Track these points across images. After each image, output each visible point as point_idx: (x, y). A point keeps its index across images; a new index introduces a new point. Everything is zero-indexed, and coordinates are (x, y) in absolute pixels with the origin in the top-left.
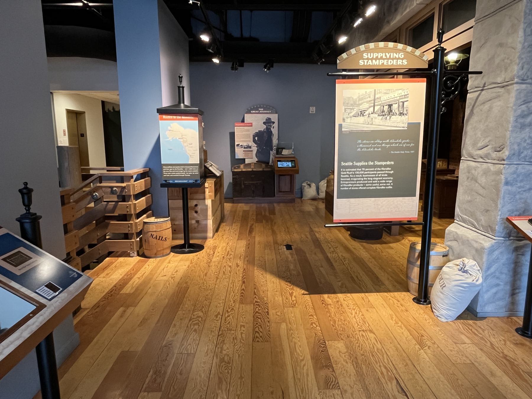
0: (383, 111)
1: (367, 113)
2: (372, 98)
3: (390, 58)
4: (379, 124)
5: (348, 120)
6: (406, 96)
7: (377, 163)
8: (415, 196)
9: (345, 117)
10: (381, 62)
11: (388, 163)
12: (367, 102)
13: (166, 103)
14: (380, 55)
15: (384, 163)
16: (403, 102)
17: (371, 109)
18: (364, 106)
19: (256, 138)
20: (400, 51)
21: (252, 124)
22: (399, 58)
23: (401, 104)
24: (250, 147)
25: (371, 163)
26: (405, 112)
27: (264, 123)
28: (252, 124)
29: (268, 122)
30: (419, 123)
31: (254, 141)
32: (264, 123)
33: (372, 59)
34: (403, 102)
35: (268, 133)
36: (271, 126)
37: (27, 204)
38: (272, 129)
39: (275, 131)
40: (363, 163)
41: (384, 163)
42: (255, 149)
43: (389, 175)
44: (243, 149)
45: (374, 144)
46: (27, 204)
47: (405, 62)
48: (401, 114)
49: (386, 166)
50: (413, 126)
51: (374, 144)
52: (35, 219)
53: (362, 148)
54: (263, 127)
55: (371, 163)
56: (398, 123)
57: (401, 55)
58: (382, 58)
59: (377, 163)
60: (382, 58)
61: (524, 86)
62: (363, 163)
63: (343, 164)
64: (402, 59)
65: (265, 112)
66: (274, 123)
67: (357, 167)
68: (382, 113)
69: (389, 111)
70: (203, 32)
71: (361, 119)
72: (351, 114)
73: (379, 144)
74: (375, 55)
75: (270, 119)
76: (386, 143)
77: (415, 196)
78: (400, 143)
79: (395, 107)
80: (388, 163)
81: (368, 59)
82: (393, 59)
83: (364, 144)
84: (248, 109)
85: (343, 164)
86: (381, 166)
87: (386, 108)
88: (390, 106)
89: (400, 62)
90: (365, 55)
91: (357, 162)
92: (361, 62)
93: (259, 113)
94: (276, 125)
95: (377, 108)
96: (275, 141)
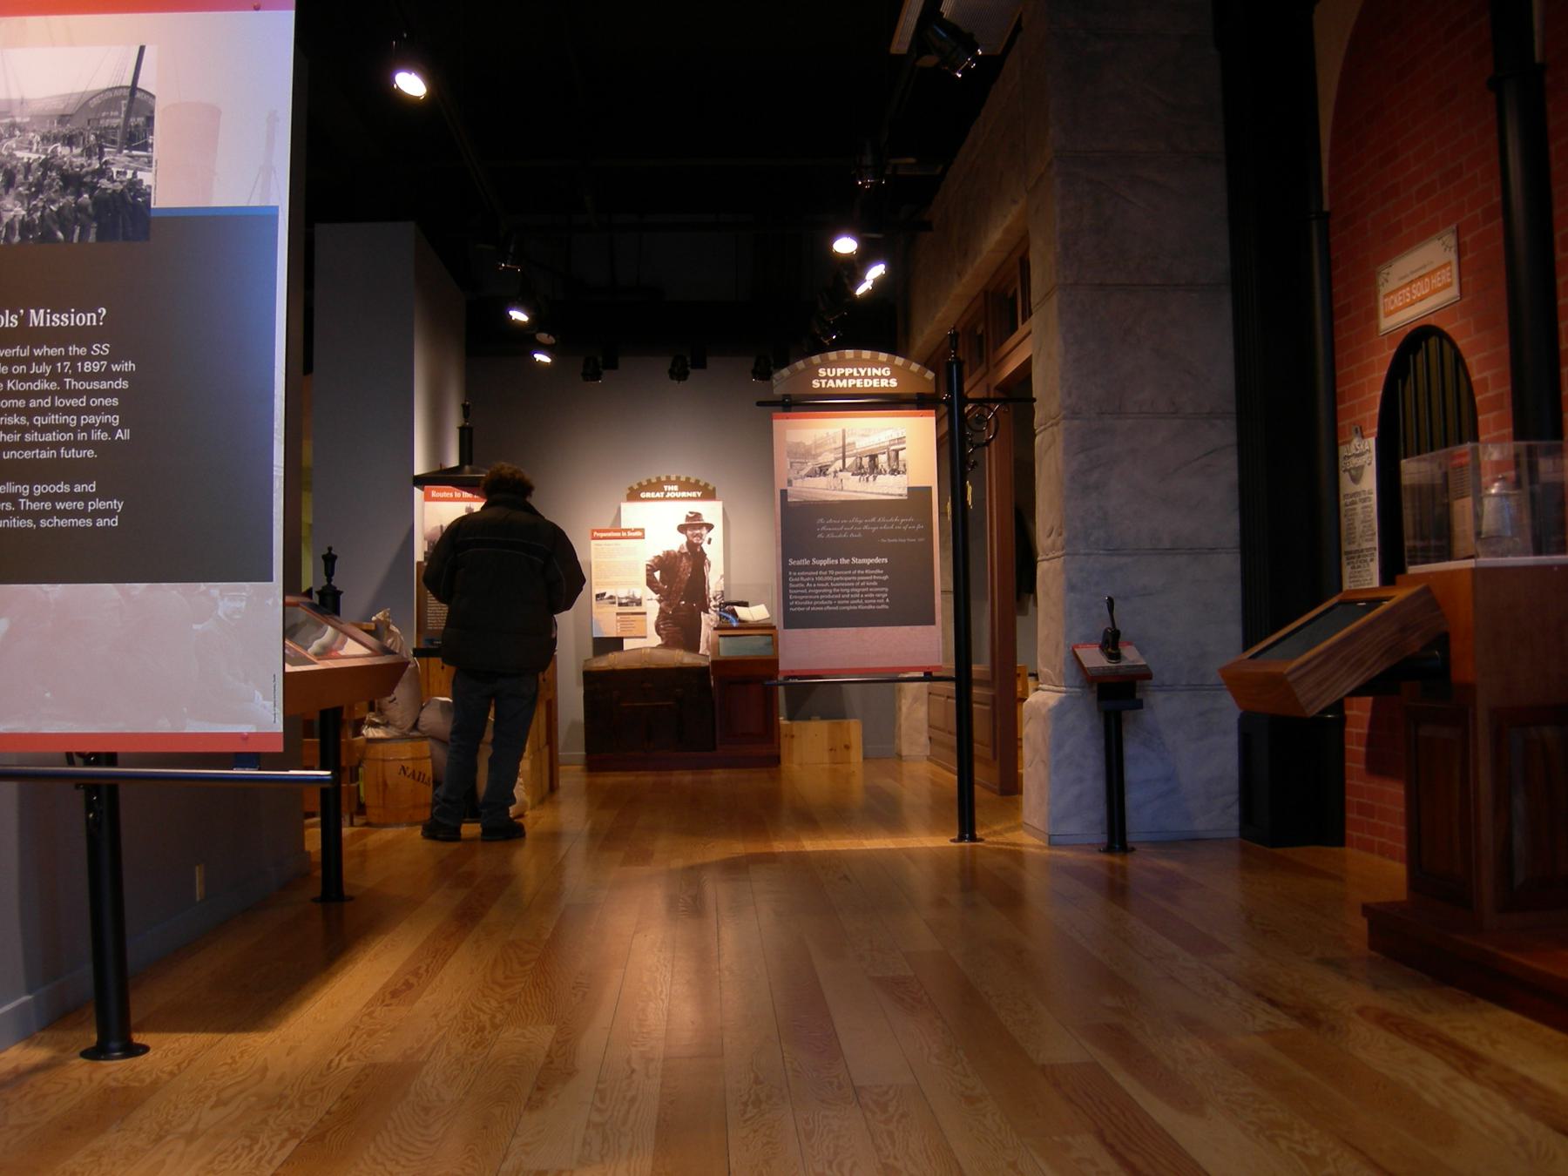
0: (861, 467)
1: (831, 470)
2: (840, 444)
3: (866, 376)
4: (855, 488)
5: (797, 484)
6: (901, 440)
7: (855, 561)
8: (933, 623)
9: (791, 476)
10: (851, 382)
11: (877, 560)
12: (831, 451)
13: (419, 469)
14: (848, 371)
15: (869, 561)
16: (897, 452)
17: (839, 464)
18: (826, 458)
19: (657, 574)
20: (882, 365)
21: (642, 530)
22: (883, 377)
23: (893, 454)
24: (639, 603)
25: (844, 561)
26: (901, 468)
27: (682, 529)
28: (642, 530)
29: (693, 524)
30: (930, 488)
31: (651, 583)
32: (682, 529)
33: (835, 378)
34: (897, 452)
35: (696, 556)
36: (701, 536)
37: (330, 573)
38: (705, 546)
39: (714, 550)
40: (828, 561)
41: (869, 561)
42: (652, 606)
43: (881, 583)
44: (616, 608)
45: (848, 525)
46: (330, 573)
47: (894, 383)
48: (894, 472)
49: (873, 566)
50: (918, 495)
51: (848, 525)
52: (336, 594)
53: (825, 533)
54: (677, 542)
55: (844, 561)
56: (888, 487)
57: (886, 371)
58: (851, 376)
59: (855, 561)
60: (851, 376)
61: (1076, 422)
62: (828, 561)
63: (792, 562)
64: (888, 378)
65: (684, 494)
66: (710, 527)
67: (817, 568)
68: (859, 471)
69: (870, 466)
70: (409, 66)
71: (821, 482)
72: (803, 473)
73: (856, 525)
74: (840, 371)
75: (697, 516)
76: (872, 525)
77: (933, 623)
78: (897, 524)
79: (882, 459)
80: (877, 560)
81: (827, 377)
82: (872, 378)
83: (830, 525)
84: (631, 489)
85: (792, 562)
86: (863, 567)
87: (866, 461)
88: (873, 458)
89: (884, 383)
90: (822, 372)
91: (818, 558)
92: (816, 384)
93: (664, 499)
94: (717, 534)
95: (849, 461)
96: (715, 580)
